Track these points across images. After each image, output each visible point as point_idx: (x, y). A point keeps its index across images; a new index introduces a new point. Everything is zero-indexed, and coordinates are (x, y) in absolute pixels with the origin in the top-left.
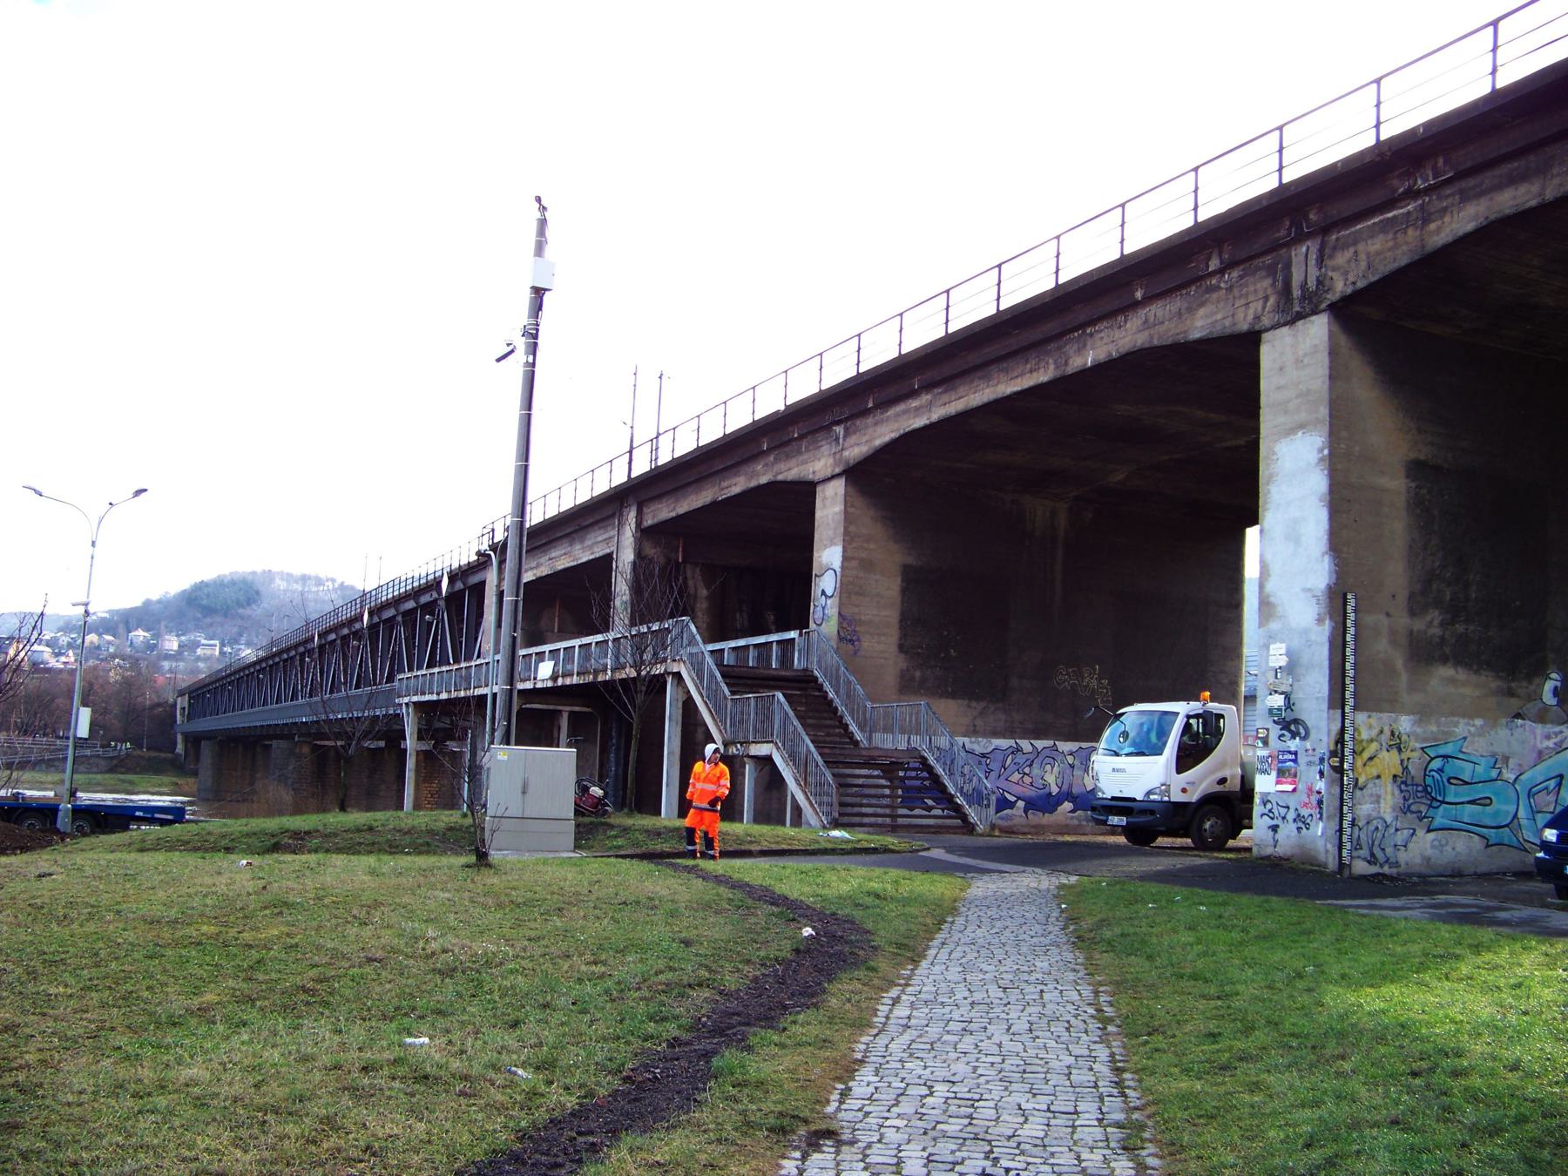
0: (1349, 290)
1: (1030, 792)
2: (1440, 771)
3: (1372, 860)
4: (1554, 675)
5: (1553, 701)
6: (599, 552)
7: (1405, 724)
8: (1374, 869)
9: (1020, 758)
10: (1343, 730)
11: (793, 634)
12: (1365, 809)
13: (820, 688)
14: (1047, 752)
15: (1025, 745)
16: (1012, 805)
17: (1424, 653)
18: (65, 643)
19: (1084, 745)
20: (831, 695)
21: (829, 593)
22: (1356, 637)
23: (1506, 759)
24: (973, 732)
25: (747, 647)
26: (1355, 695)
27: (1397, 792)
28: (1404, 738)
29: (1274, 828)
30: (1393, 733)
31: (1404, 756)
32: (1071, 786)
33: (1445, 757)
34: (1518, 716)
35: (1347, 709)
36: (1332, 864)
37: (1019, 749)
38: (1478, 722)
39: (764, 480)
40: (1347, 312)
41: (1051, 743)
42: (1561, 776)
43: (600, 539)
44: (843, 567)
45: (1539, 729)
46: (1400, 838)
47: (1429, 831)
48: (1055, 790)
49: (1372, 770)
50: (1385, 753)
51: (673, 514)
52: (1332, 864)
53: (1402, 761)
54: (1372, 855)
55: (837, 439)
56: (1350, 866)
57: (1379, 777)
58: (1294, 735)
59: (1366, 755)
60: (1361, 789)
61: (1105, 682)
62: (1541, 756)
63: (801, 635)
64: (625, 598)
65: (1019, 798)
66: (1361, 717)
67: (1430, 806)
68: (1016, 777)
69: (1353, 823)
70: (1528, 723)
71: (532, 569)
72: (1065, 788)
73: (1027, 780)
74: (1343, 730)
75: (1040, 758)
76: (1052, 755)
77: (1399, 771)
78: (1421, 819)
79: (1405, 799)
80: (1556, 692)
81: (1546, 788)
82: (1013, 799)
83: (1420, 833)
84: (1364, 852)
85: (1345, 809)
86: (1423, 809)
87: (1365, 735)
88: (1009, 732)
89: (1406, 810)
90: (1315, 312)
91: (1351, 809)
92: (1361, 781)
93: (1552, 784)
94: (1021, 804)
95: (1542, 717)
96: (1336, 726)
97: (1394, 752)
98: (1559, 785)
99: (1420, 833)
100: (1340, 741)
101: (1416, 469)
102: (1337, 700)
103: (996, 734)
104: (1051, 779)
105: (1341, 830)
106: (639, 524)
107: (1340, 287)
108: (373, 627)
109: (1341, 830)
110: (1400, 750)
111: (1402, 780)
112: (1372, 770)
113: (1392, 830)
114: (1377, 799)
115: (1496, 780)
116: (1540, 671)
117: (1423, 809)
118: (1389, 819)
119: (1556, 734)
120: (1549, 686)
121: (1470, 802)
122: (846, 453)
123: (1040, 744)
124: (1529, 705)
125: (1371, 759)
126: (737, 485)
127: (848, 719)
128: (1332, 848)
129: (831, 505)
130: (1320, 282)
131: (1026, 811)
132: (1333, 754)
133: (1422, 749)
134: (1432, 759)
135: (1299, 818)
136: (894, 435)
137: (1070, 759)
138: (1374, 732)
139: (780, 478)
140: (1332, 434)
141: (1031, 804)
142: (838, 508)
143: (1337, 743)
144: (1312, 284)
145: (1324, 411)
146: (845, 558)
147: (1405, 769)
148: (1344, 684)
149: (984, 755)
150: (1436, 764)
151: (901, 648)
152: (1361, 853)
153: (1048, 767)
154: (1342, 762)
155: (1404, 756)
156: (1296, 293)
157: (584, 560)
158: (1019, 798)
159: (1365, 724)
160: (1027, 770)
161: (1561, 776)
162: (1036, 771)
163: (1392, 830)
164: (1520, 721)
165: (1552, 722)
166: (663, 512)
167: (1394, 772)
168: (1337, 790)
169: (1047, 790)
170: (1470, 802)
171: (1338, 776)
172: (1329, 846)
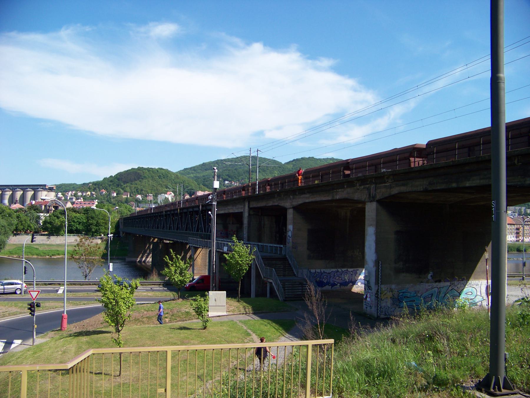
0: (379, 198)
1: (341, 281)
2: (401, 295)
3: (385, 314)
4: (431, 273)
5: (431, 278)
6: (240, 210)
7: (393, 286)
8: (386, 316)
9: (338, 273)
10: (378, 289)
11: (282, 246)
12: (383, 304)
13: (288, 260)
14: (346, 271)
15: (340, 270)
16: (337, 285)
17: (398, 271)
18: (80, 195)
19: (355, 269)
20: (290, 262)
21: (290, 236)
22: (381, 270)
23: (418, 292)
24: (327, 268)
25: (273, 246)
26: (381, 282)
27: (391, 301)
28: (393, 289)
29: (367, 308)
30: (390, 289)
31: (393, 293)
32: (352, 279)
33: (404, 292)
34: (422, 282)
35: (379, 285)
36: (376, 316)
37: (338, 271)
38: (411, 284)
39: (276, 204)
40: (379, 202)
41: (346, 269)
42: (432, 294)
43: (240, 207)
44: (293, 231)
45: (427, 284)
46: (392, 310)
47: (399, 308)
48: (347, 280)
49: (385, 296)
50: (388, 293)
51: (257, 206)
52: (376, 316)
53: (393, 294)
54: (385, 313)
55: (291, 199)
56: (380, 316)
57: (387, 298)
58: (370, 289)
59: (384, 294)
60: (383, 300)
61: (360, 253)
62: (427, 290)
63: (284, 246)
64: (246, 225)
65: (338, 283)
66: (383, 286)
67: (399, 303)
68: (337, 278)
69: (381, 307)
70: (424, 283)
71: (223, 210)
72: (350, 280)
73: (340, 278)
74: (378, 289)
75: (344, 273)
76: (347, 272)
77: (392, 296)
78: (397, 306)
79: (393, 302)
80: (431, 276)
81: (429, 297)
82: (337, 283)
83: (397, 308)
84: (384, 313)
85: (379, 305)
86: (398, 303)
87: (384, 289)
88: (335, 267)
89: (393, 304)
90: (374, 201)
91: (380, 305)
92: (383, 299)
93: (430, 296)
94: (339, 284)
95: (428, 282)
96: (376, 289)
97: (391, 292)
98: (432, 296)
99: (397, 308)
100: (378, 291)
101: (397, 233)
102: (377, 282)
103: (332, 268)
104: (346, 278)
105: (378, 309)
106: (249, 207)
107: (378, 197)
108: (181, 213)
109: (378, 309)
110: (392, 292)
111: (393, 298)
112: (385, 296)
113: (390, 308)
114: (387, 302)
115: (416, 296)
116: (427, 272)
117: (398, 303)
118: (389, 306)
119: (431, 285)
120: (430, 275)
121: (410, 301)
122: (293, 203)
123: (343, 270)
124: (425, 280)
125: (385, 294)
126: (270, 203)
127: (294, 269)
128: (376, 313)
129: (290, 214)
130: (375, 195)
131: (340, 286)
132: (376, 294)
133: (398, 291)
134: (400, 293)
135: (370, 306)
136: (302, 202)
137: (351, 273)
138: (386, 289)
139: (280, 205)
140: (376, 228)
141: (341, 284)
142: (292, 216)
143: (377, 292)
144: (374, 194)
145: (375, 223)
146: (293, 228)
147: (393, 296)
148: (378, 280)
149: (329, 273)
150: (401, 294)
151: (308, 249)
152: (383, 313)
153: (346, 275)
154: (378, 295)
155: (393, 293)
156: (371, 196)
157: (236, 211)
158: (338, 283)
159: (384, 287)
160: (340, 276)
161: (432, 294)
162: (342, 276)
163: (390, 308)
164: (422, 283)
165: (430, 283)
166: (254, 205)
167: (391, 296)
168: (377, 301)
169: (345, 281)
170: (410, 301)
171: (377, 298)
172: (375, 313)
